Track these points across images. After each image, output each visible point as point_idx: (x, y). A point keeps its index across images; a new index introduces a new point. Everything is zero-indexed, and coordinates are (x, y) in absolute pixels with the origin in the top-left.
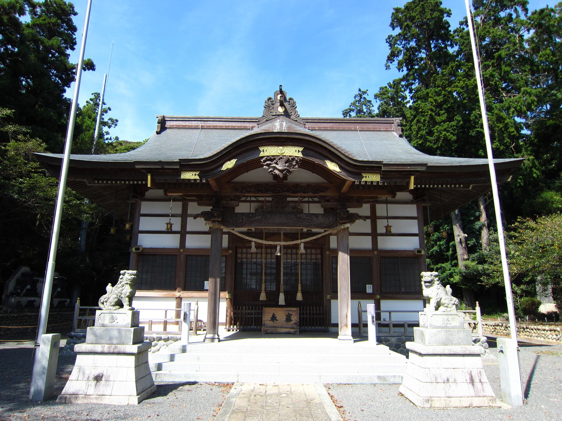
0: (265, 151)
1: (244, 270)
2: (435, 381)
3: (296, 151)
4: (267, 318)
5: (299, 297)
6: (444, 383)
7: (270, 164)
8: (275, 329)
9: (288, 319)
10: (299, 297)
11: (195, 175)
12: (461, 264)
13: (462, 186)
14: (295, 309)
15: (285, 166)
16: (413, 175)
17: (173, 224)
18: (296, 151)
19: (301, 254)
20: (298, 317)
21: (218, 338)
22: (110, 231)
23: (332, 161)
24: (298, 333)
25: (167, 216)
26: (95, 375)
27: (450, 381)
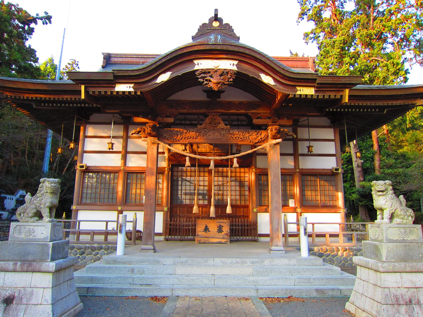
0: (199, 64)
1: (179, 186)
2: (396, 303)
3: (230, 64)
4: (200, 229)
5: (229, 210)
6: (407, 305)
7: (205, 77)
8: (207, 239)
9: (220, 230)
10: (229, 210)
11: (130, 87)
12: (357, 184)
13: (377, 110)
14: (225, 221)
15: (220, 79)
16: (348, 88)
17: (114, 144)
18: (230, 64)
19: (235, 168)
20: (229, 228)
21: (154, 249)
22: (57, 151)
23: (267, 74)
24: (229, 242)
25: (109, 137)
26: (5, 298)
27: (413, 302)
